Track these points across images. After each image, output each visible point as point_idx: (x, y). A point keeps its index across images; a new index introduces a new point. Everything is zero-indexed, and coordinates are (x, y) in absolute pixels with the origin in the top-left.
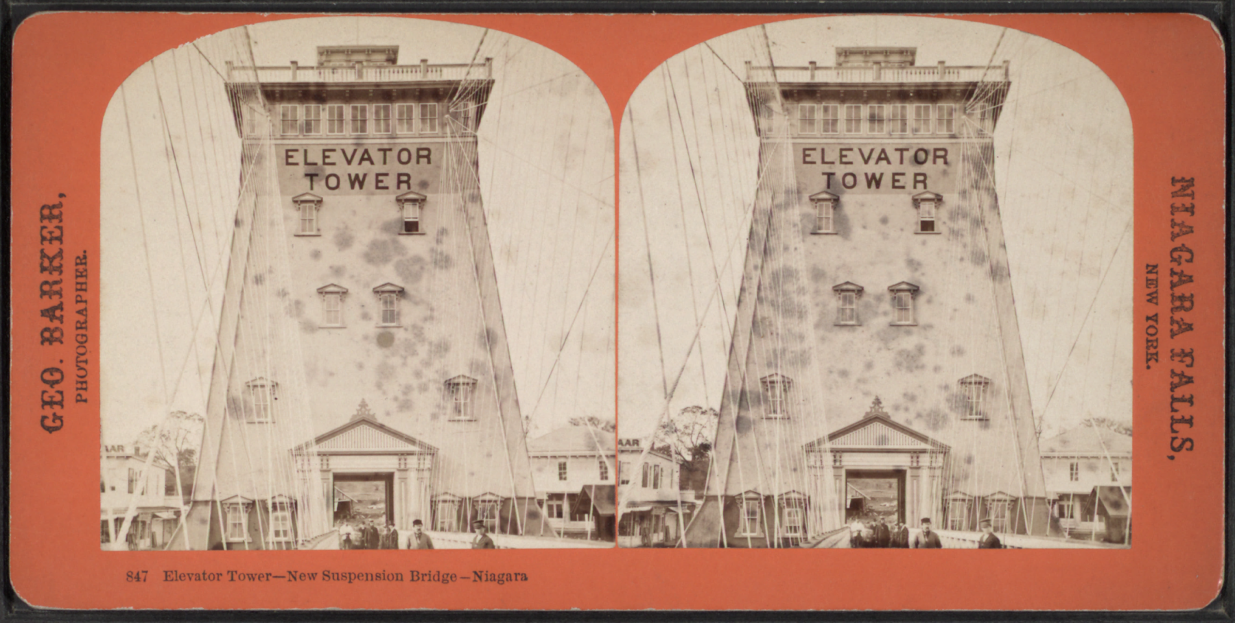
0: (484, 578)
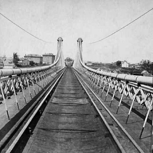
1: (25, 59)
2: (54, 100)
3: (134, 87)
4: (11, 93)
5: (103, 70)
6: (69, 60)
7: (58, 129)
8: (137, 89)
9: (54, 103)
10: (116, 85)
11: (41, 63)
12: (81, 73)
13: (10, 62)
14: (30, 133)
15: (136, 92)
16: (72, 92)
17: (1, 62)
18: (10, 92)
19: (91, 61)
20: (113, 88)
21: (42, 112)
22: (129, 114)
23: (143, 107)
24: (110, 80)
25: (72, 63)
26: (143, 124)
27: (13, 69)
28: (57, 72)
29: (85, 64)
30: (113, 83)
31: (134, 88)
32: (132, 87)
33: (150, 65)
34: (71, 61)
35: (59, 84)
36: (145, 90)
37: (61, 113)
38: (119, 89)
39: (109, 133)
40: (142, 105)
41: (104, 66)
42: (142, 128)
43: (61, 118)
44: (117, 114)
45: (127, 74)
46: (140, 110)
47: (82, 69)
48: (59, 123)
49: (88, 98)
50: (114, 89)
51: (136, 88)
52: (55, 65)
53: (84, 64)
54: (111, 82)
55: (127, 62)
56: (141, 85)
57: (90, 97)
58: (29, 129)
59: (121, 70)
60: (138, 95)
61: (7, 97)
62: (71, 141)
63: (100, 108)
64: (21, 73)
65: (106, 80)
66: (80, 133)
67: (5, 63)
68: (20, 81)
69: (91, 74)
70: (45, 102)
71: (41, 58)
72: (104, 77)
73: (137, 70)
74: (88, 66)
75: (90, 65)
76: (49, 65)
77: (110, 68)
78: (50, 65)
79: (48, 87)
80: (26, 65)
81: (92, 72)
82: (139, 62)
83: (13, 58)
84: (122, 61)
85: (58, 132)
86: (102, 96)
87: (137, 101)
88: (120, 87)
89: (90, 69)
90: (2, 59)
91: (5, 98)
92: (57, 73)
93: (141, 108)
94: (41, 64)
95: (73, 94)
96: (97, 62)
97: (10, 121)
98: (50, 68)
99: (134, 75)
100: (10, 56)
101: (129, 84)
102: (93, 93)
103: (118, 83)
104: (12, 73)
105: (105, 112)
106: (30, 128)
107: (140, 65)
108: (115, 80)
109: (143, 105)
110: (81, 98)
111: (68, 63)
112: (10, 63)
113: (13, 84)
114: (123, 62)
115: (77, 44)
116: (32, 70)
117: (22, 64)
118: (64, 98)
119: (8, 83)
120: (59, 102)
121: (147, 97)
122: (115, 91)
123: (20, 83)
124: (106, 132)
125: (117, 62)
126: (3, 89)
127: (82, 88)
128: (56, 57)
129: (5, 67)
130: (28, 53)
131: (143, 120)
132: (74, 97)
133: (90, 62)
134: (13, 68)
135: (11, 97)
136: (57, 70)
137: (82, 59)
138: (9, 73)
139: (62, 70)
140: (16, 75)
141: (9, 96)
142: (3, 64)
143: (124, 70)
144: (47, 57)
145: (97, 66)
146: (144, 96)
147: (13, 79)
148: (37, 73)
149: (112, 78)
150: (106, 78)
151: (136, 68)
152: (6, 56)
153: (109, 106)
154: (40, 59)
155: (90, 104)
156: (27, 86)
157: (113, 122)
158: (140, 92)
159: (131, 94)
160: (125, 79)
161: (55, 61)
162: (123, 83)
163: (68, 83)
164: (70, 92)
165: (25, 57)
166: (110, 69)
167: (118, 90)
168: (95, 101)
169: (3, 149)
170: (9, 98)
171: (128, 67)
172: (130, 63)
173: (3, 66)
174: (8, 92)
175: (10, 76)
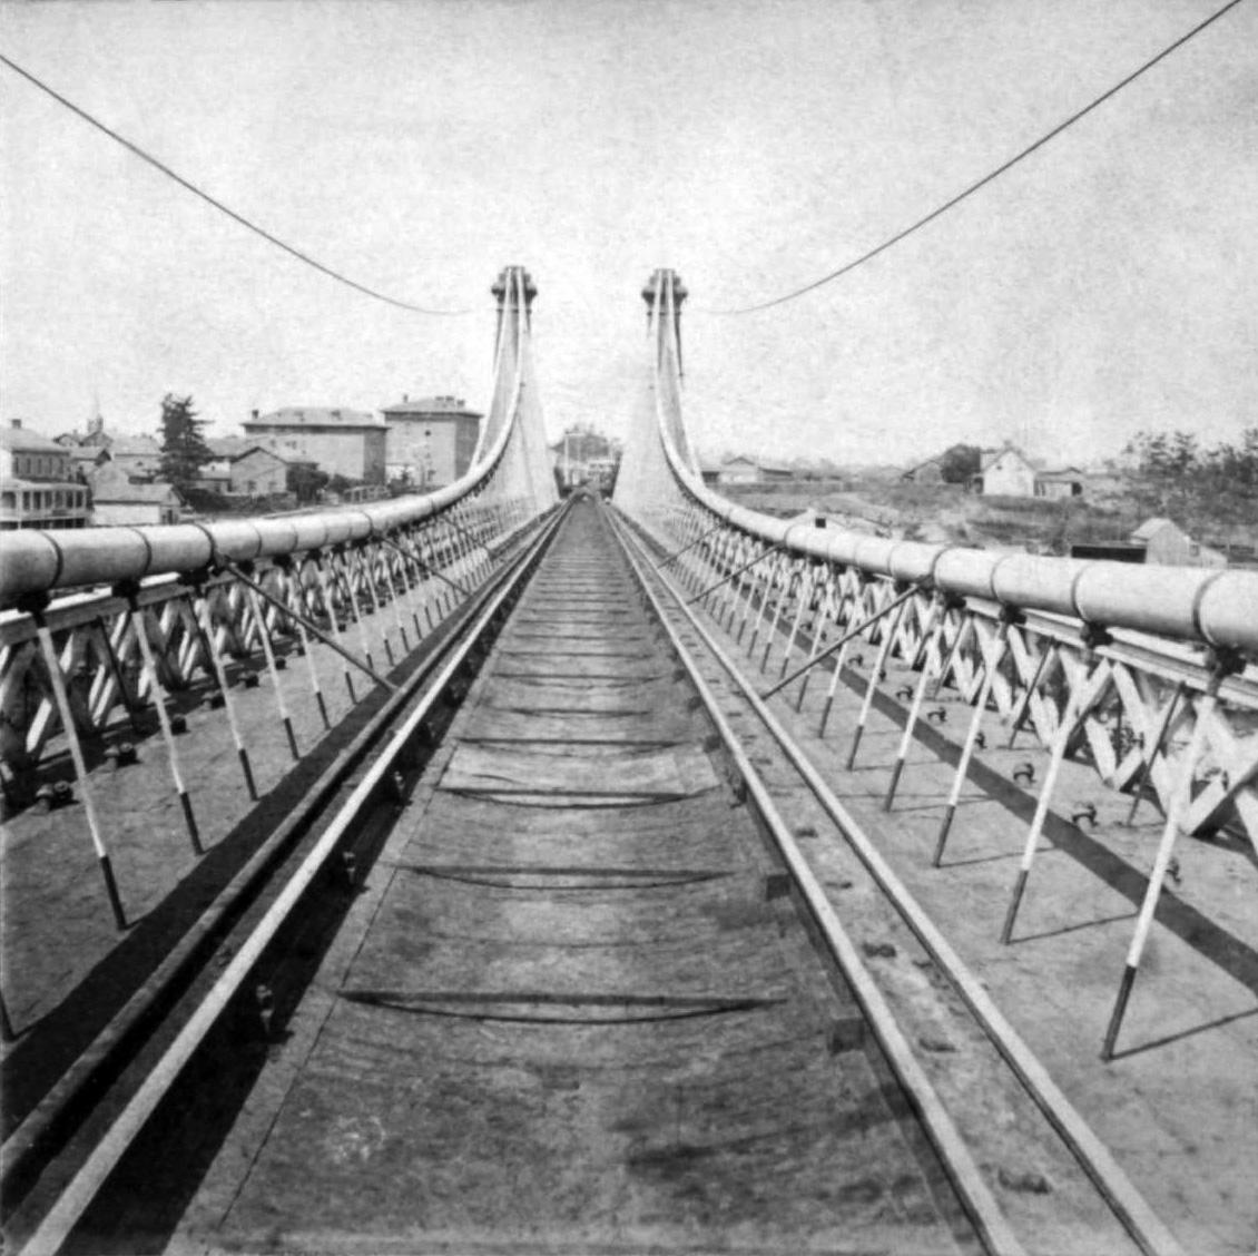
1: (254, 445)
2: (462, 765)
5: (841, 517)
6: (585, 445)
9: (457, 792)
11: (375, 474)
12: (672, 547)
13: (144, 474)
15: (1084, 690)
16: (600, 699)
18: (129, 708)
20: (909, 656)
21: (364, 870)
25: (608, 470)
29: (710, 477)
32: (1051, 653)
33: (1198, 474)
34: (605, 451)
38: (962, 667)
39: (857, 1015)
41: (849, 488)
42: (1121, 972)
44: (937, 865)
49: (716, 743)
52: (476, 488)
57: (734, 742)
59: (983, 519)
61: (112, 751)
62: (576, 1086)
63: (800, 824)
64: (212, 559)
66: (594, 611)
67: (111, 480)
70: (394, 782)
71: (375, 435)
73: (1100, 513)
74: (736, 493)
75: (739, 480)
76: (430, 490)
77: (897, 501)
79: (344, 743)
82: (1114, 451)
83: (160, 439)
85: (480, 1018)
86: (831, 726)
88: (963, 654)
89: (740, 515)
90: (76, 451)
94: (380, 483)
95: (597, 601)
100: (140, 426)
104: (141, 561)
105: (841, 852)
107: (1117, 478)
110: (666, 745)
111: (575, 470)
112: (135, 480)
114: (991, 451)
116: (327, 529)
117: (230, 489)
118: (536, 748)
120: (492, 784)
124: (836, 1014)
128: (483, 423)
129: (101, 514)
131: (1132, 908)
133: (742, 460)
135: (142, 750)
139: (533, 525)
140: (172, 576)
141: (126, 746)
142: (90, 494)
145: (796, 490)
147: (158, 609)
151: (1090, 501)
152: (107, 428)
153: (882, 801)
154: (369, 443)
163: (569, 630)
164: (582, 705)
165: (250, 428)
166: (892, 513)
167: (949, 680)
169: (53, 1162)
170: (127, 759)
171: (1030, 492)
172: (1043, 462)
173: (90, 506)
174: (119, 715)
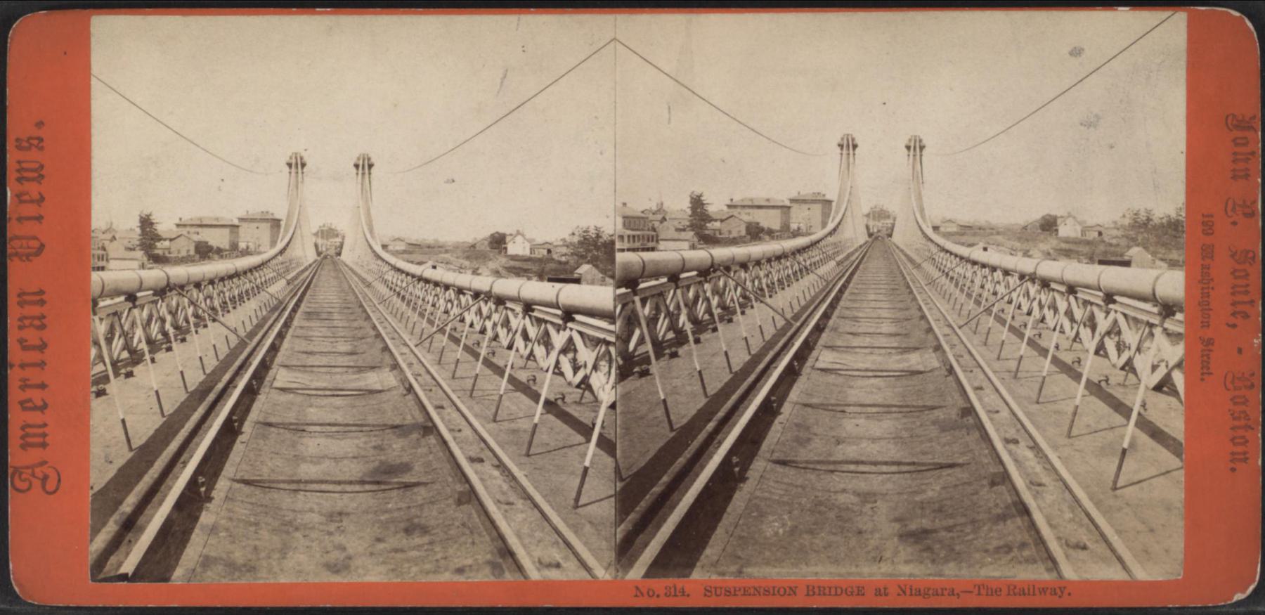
0: (908, 592)
2: (280, 376)
3: (552, 323)
4: (136, 358)
7: (299, 482)
8: (561, 332)
9: (822, 370)
10: (489, 317)
11: (234, 246)
13: (682, 227)
14: (737, 475)
15: (559, 340)
16: (886, 328)
17: (100, 245)
18: (130, 352)
19: (402, 235)
22: (536, 420)
23: (583, 394)
24: (467, 300)
26: (585, 455)
27: (138, 271)
28: (289, 277)
30: (479, 312)
31: (550, 328)
33: (1154, 227)
35: (296, 323)
36: (588, 336)
37: (846, 405)
38: (502, 332)
40: (578, 386)
43: (305, 440)
45: (525, 278)
46: (574, 406)
47: (374, 265)
48: (299, 459)
50: (483, 331)
51: (559, 329)
53: (381, 248)
54: (474, 309)
55: (523, 235)
56: (574, 316)
58: (200, 481)
60: (564, 351)
65: (456, 302)
68: (166, 313)
69: (402, 281)
70: (253, 385)
71: (785, 209)
72: (447, 293)
73: (560, 263)
74: (396, 253)
75: (949, 230)
76: (259, 253)
77: (468, 258)
78: (265, 252)
80: (184, 253)
81: (408, 274)
82: (1117, 216)
84: (508, 233)
85: (296, 491)
87: (562, 374)
88: (502, 326)
91: (117, 375)
92: (288, 283)
93: (578, 400)
94: (235, 250)
95: (891, 335)
96: (425, 240)
97: (134, 456)
98: (813, 244)
99: (550, 280)
101: (535, 314)
102: (412, 351)
103: (496, 311)
104: (680, 265)
105: (994, 396)
106: (201, 479)
108: (486, 302)
109: (583, 386)
111: (875, 225)
113: (142, 325)
115: (839, 156)
119: (123, 321)
121: (596, 359)
122: (487, 339)
123: (163, 321)
124: (459, 488)
125: (492, 235)
126: (109, 341)
127: (372, 333)
128: (834, 204)
129: (112, 264)
130: (188, 215)
132: (892, 348)
133: (950, 221)
134: (140, 269)
135: (681, 351)
136: (287, 271)
137: (371, 231)
138: (125, 287)
140: (694, 273)
143: (517, 264)
144: (256, 225)
146: (586, 355)
147: (142, 307)
148: (221, 283)
149: (476, 295)
150: (453, 296)
152: (665, 206)
155: (402, 388)
156: (188, 331)
157: (482, 449)
158: (570, 340)
159: (540, 351)
160: (493, 291)
161: (282, 240)
162: (512, 310)
163: (872, 297)
165: (729, 206)
166: (467, 263)
168: (960, 359)
172: (534, 240)
173: (107, 260)
174: (671, 335)
175: (131, 298)
